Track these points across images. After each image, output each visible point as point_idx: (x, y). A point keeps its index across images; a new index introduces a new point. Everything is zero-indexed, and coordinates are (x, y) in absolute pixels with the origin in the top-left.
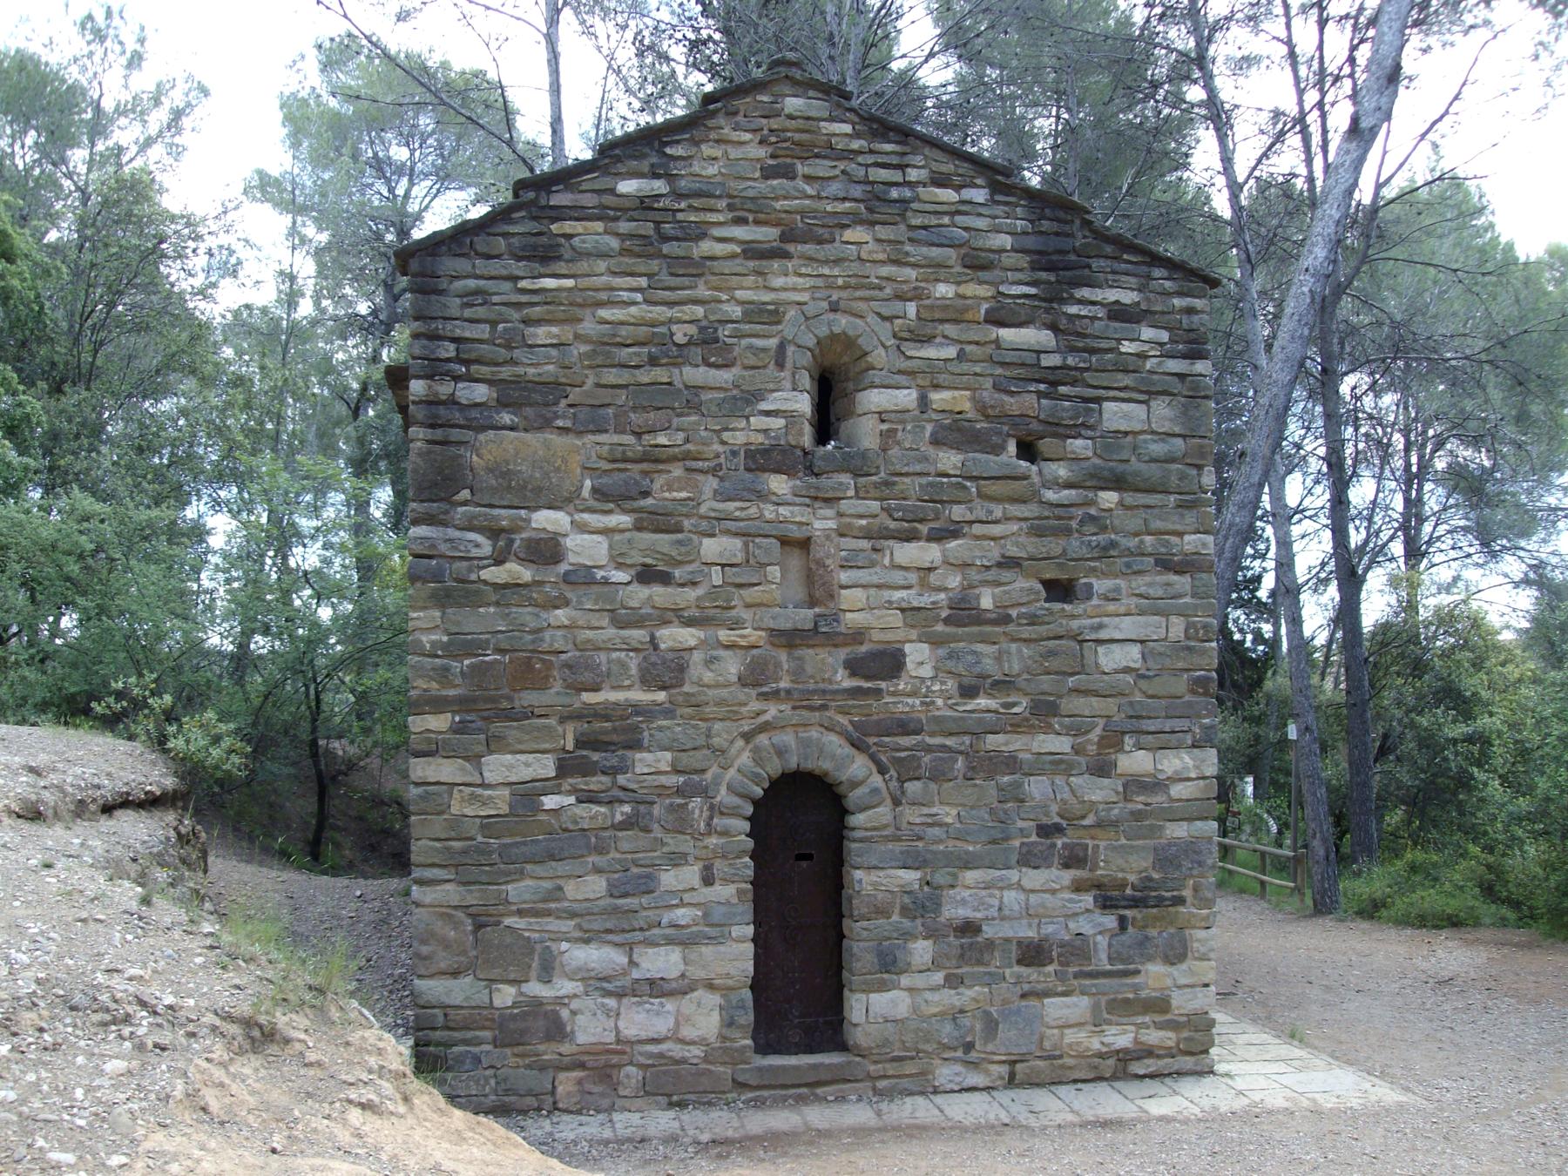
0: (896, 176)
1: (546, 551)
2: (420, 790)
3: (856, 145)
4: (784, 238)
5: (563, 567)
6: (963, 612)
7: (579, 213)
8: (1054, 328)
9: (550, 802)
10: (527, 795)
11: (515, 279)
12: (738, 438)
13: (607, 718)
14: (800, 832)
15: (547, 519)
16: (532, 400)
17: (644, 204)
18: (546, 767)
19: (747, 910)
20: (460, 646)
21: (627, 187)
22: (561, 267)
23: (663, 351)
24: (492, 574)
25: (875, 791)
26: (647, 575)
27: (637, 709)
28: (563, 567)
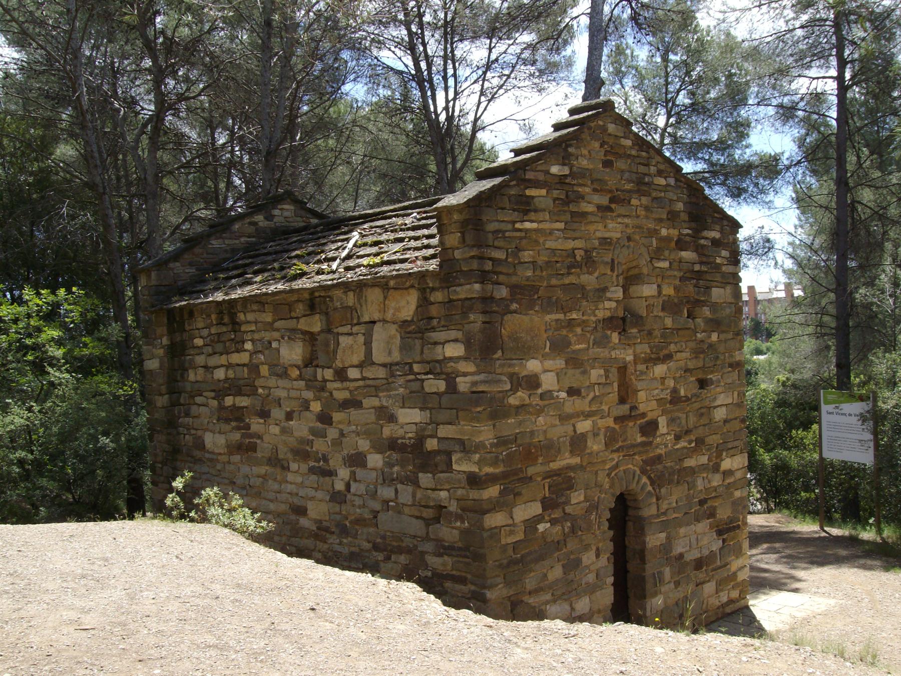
0: (510, 227)
1: (532, 382)
2: (489, 533)
3: (634, 153)
4: (612, 200)
5: (540, 391)
6: (675, 399)
7: (537, 184)
8: (696, 251)
9: (541, 527)
10: (531, 524)
11: (514, 222)
12: (600, 314)
13: (559, 475)
14: (624, 516)
15: (533, 365)
16: (525, 294)
17: (561, 180)
18: (536, 509)
19: (611, 569)
20: (502, 442)
21: (555, 170)
22: (532, 215)
23: (573, 264)
24: (513, 401)
25: (649, 492)
26: (573, 392)
27: (569, 468)
28: (540, 391)
